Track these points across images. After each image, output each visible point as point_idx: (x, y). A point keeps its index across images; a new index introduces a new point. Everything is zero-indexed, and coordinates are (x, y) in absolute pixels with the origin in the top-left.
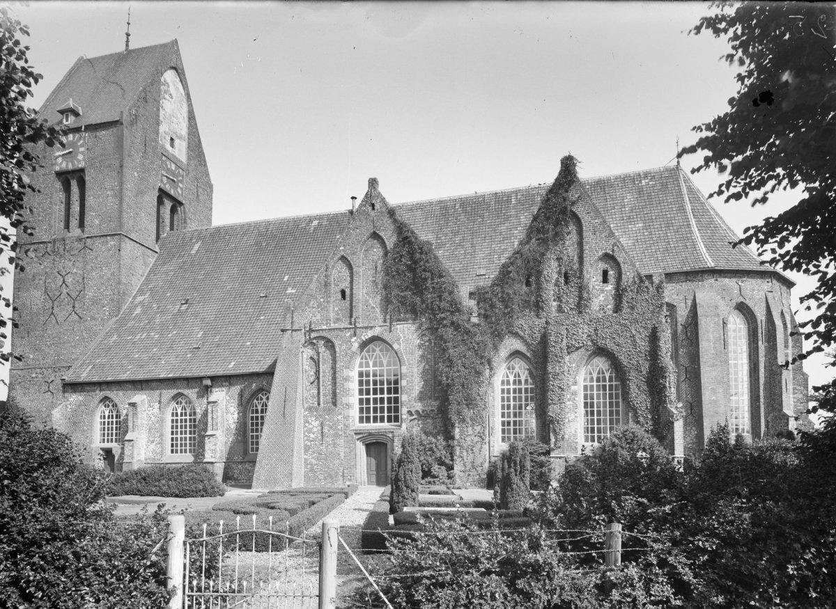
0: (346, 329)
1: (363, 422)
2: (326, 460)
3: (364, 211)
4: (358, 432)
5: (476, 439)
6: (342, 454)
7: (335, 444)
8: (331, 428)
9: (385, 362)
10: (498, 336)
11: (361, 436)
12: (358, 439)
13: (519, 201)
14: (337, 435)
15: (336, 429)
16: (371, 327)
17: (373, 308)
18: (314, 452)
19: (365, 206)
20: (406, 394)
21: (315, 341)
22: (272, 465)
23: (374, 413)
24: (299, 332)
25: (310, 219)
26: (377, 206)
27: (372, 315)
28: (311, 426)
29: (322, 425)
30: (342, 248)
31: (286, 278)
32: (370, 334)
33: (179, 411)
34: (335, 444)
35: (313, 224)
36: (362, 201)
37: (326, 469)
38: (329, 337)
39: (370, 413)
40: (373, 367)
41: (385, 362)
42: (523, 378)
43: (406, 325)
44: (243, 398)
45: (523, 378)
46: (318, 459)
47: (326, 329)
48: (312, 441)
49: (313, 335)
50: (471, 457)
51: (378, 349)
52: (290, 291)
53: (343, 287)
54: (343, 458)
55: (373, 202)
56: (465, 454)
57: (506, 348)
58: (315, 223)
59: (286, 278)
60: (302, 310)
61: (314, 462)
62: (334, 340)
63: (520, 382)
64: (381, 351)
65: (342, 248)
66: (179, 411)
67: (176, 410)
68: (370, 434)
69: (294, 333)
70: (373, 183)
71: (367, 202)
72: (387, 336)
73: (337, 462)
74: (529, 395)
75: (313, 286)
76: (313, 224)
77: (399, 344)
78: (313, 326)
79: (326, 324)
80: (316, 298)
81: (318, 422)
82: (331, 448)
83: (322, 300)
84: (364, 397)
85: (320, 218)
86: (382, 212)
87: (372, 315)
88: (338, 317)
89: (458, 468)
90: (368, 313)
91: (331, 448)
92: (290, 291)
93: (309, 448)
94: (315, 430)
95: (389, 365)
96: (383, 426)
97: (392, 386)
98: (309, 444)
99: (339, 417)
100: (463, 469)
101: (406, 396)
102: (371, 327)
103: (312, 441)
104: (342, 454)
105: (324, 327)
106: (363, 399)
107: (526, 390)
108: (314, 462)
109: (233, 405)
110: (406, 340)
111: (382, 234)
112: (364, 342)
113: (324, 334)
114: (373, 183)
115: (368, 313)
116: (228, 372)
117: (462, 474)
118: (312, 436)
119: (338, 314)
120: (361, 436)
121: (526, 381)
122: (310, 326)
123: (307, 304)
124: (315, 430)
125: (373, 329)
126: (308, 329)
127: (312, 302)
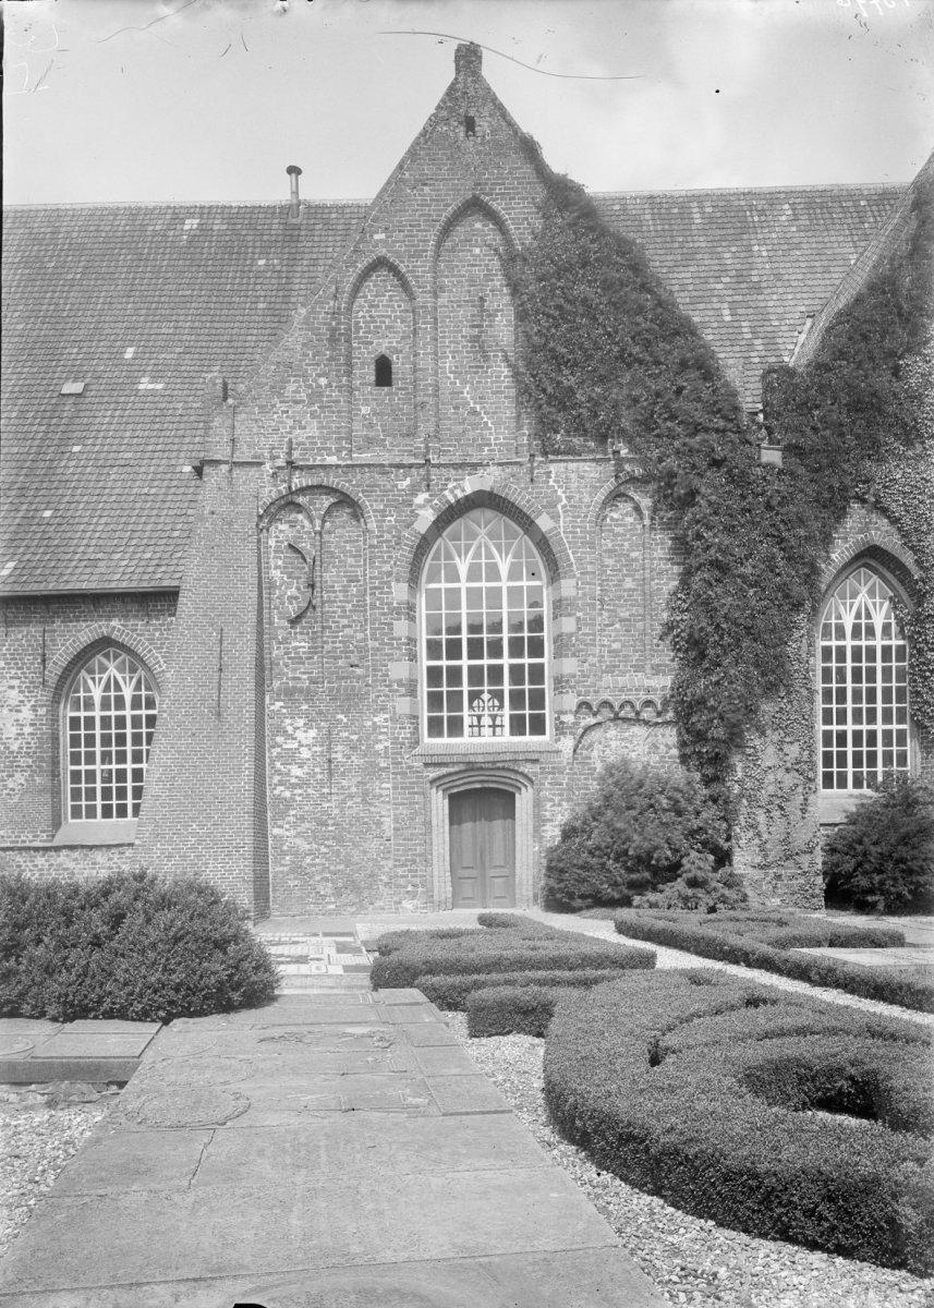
0: (399, 466)
1: (523, 733)
2: (339, 839)
3: (445, 136)
4: (436, 760)
5: (789, 780)
6: (388, 824)
7: (366, 794)
8: (353, 748)
9: (504, 568)
10: (834, 506)
11: (444, 770)
12: (432, 782)
13: (710, 220)
14: (372, 771)
15: (370, 752)
16: (475, 466)
17: (474, 412)
18: (302, 819)
19: (446, 121)
20: (574, 655)
21: (301, 500)
22: (184, 857)
23: (854, 702)
24: (253, 471)
25: (177, 214)
26: (483, 126)
27: (471, 434)
28: (293, 745)
29: (328, 740)
30: (380, 236)
31: (129, 353)
32: (470, 485)
33: (128, 693)
34: (366, 794)
35: (186, 227)
36: (439, 108)
37: (342, 867)
38: (346, 487)
39: (884, 710)
40: (469, 579)
41: (504, 568)
42: (878, 621)
43: (572, 466)
44: (50, 665)
45: (878, 621)
46: (315, 837)
47: (338, 466)
48: (294, 786)
49: (299, 480)
50: (779, 828)
51: (864, 590)
52: (145, 384)
53: (383, 350)
54: (389, 833)
55: (471, 114)
56: (762, 818)
57: (845, 539)
58: (191, 224)
59: (129, 353)
60: (261, 407)
61: (304, 846)
62: (361, 498)
63: (870, 631)
64: (491, 536)
65: (380, 236)
66: (128, 693)
67: (869, 616)
68: (471, 767)
69: (237, 472)
70: (468, 58)
71: (451, 110)
72: (520, 496)
73: (373, 846)
74: (894, 664)
75: (294, 338)
76: (186, 227)
77: (555, 517)
78: (296, 454)
79: (339, 451)
80: (305, 376)
81: (313, 733)
82: (354, 807)
83: (323, 381)
84: (444, 663)
85: (205, 212)
86: (497, 144)
87: (471, 434)
88: (372, 434)
89: (743, 861)
90: (460, 428)
91: (354, 807)
92: (145, 384)
93: (288, 807)
94: (305, 753)
95: (514, 574)
96: (458, 745)
97: (526, 634)
98: (287, 794)
99: (379, 719)
100: (758, 860)
101: (574, 660)
102: (475, 466)
103: (294, 786)
104: (388, 824)
105: (332, 460)
106: (830, 647)
107: (886, 650)
108: (304, 846)
109: (16, 682)
110: (574, 508)
111: (497, 206)
112: (451, 506)
113: (332, 480)
114: (468, 58)
115: (460, 428)
116: (35, 587)
117: (757, 874)
118: (296, 771)
119: (371, 426)
120: (444, 770)
121: (886, 628)
122: (289, 454)
123: (277, 390)
124: (305, 753)
125: (481, 471)
126: (281, 462)
127: (291, 387)
